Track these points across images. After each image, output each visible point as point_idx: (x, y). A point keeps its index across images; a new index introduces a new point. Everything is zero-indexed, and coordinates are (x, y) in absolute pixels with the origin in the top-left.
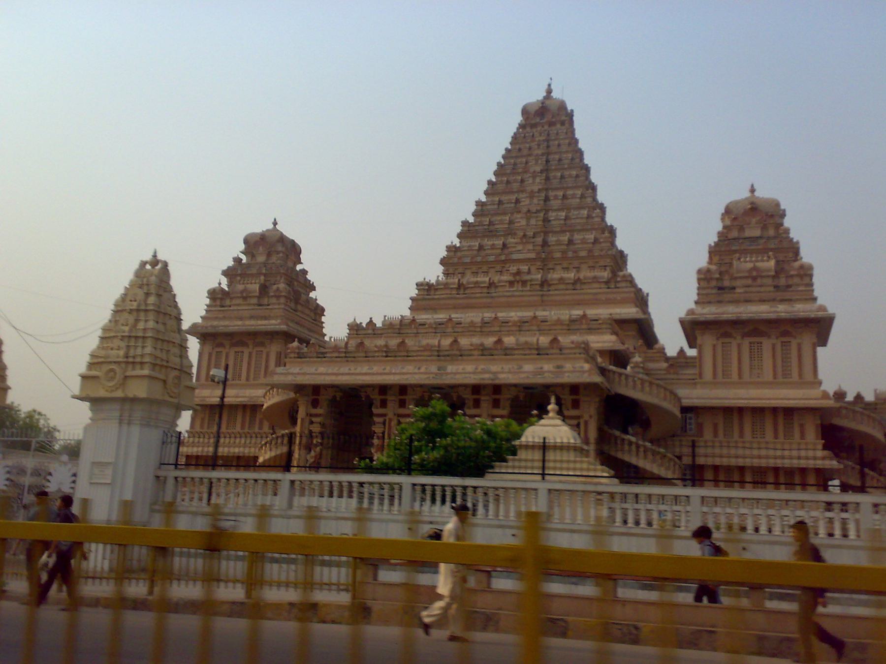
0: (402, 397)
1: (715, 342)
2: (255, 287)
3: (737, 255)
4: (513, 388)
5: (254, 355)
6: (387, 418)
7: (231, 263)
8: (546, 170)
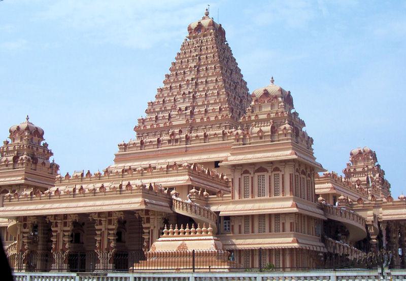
0: (65, 221)
1: (240, 177)
2: (267, 128)
3: (254, 123)
4: (117, 213)
5: (242, 180)
6: (150, 229)
8: (198, 66)
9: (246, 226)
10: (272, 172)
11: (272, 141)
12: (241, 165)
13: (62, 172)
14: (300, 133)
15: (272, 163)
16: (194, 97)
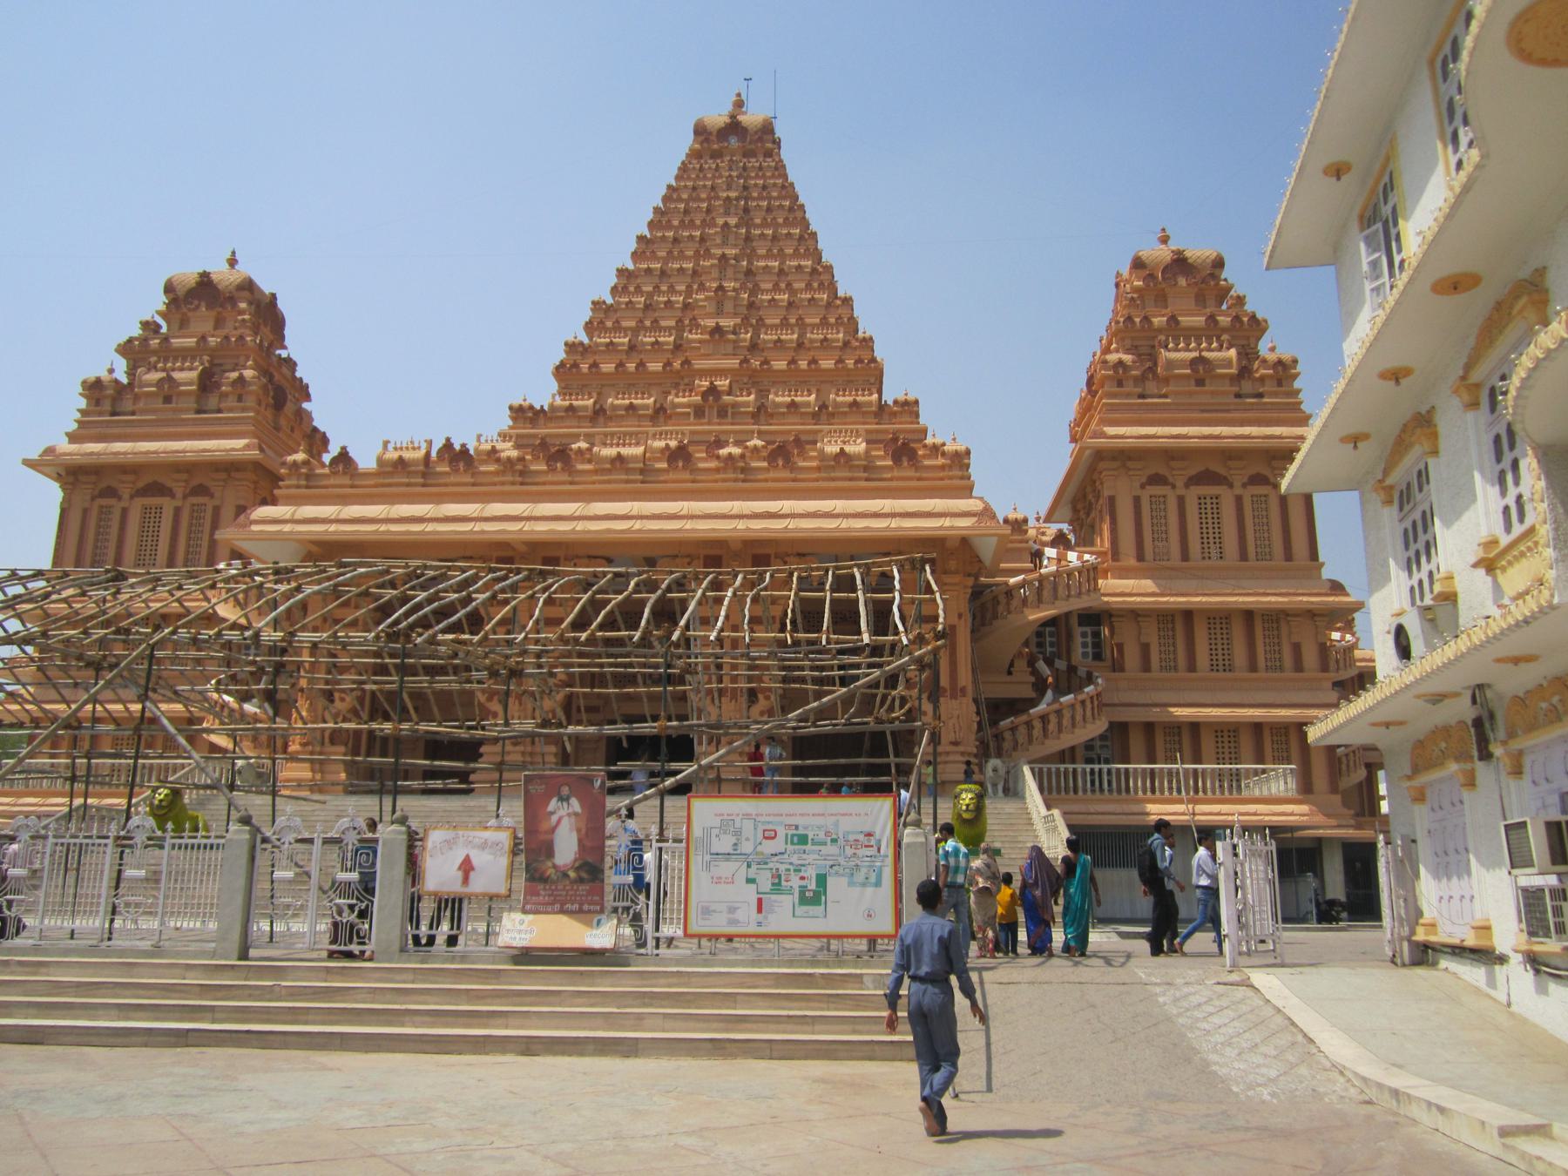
2: (187, 376)
3: (153, 359)
7: (137, 331)
10: (185, 497)
11: (199, 412)
14: (289, 408)
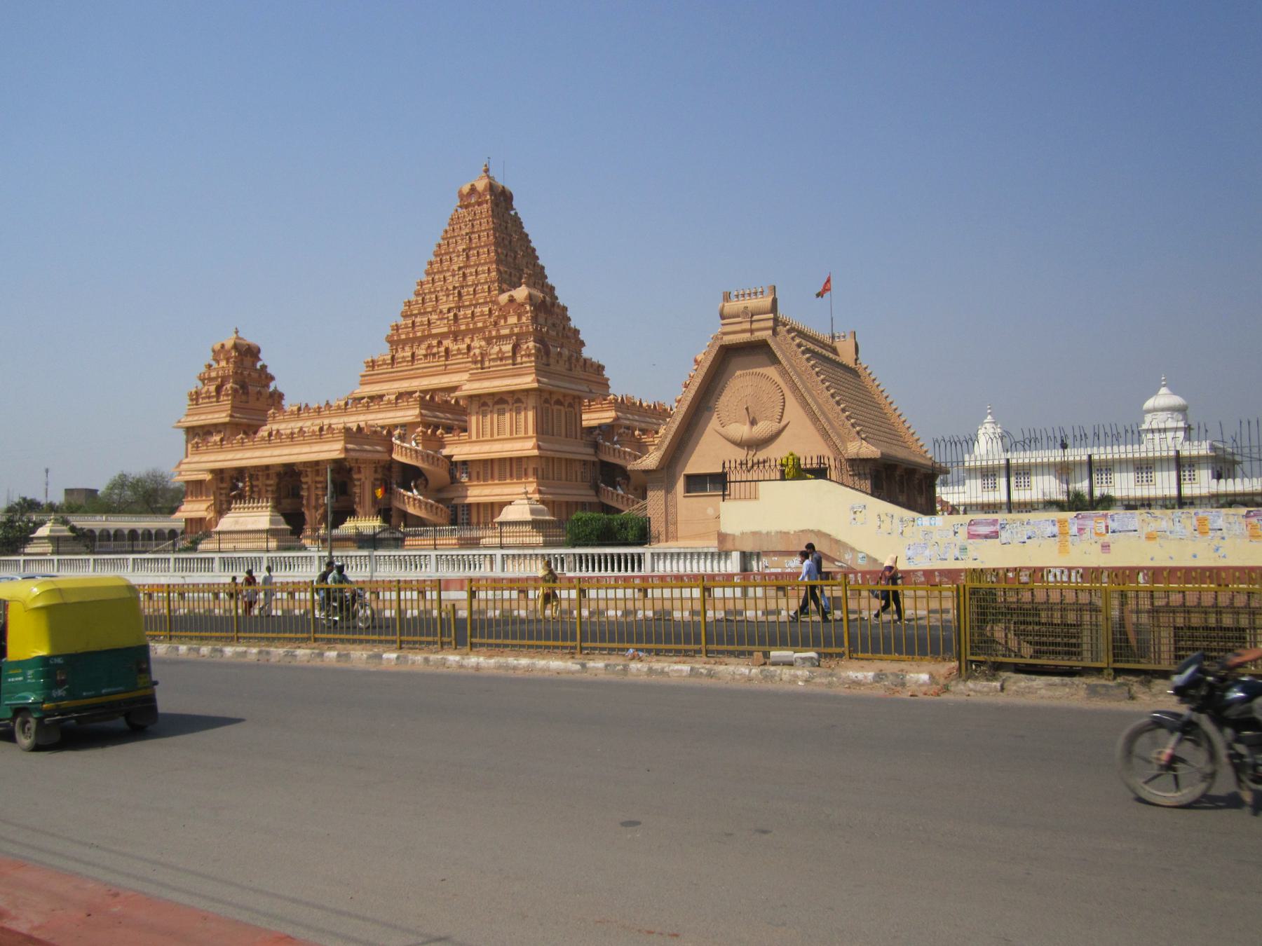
2: (507, 348)
8: (467, 250)
9: (485, 473)
12: (479, 396)
13: (289, 404)
15: (513, 392)
16: (459, 293)
